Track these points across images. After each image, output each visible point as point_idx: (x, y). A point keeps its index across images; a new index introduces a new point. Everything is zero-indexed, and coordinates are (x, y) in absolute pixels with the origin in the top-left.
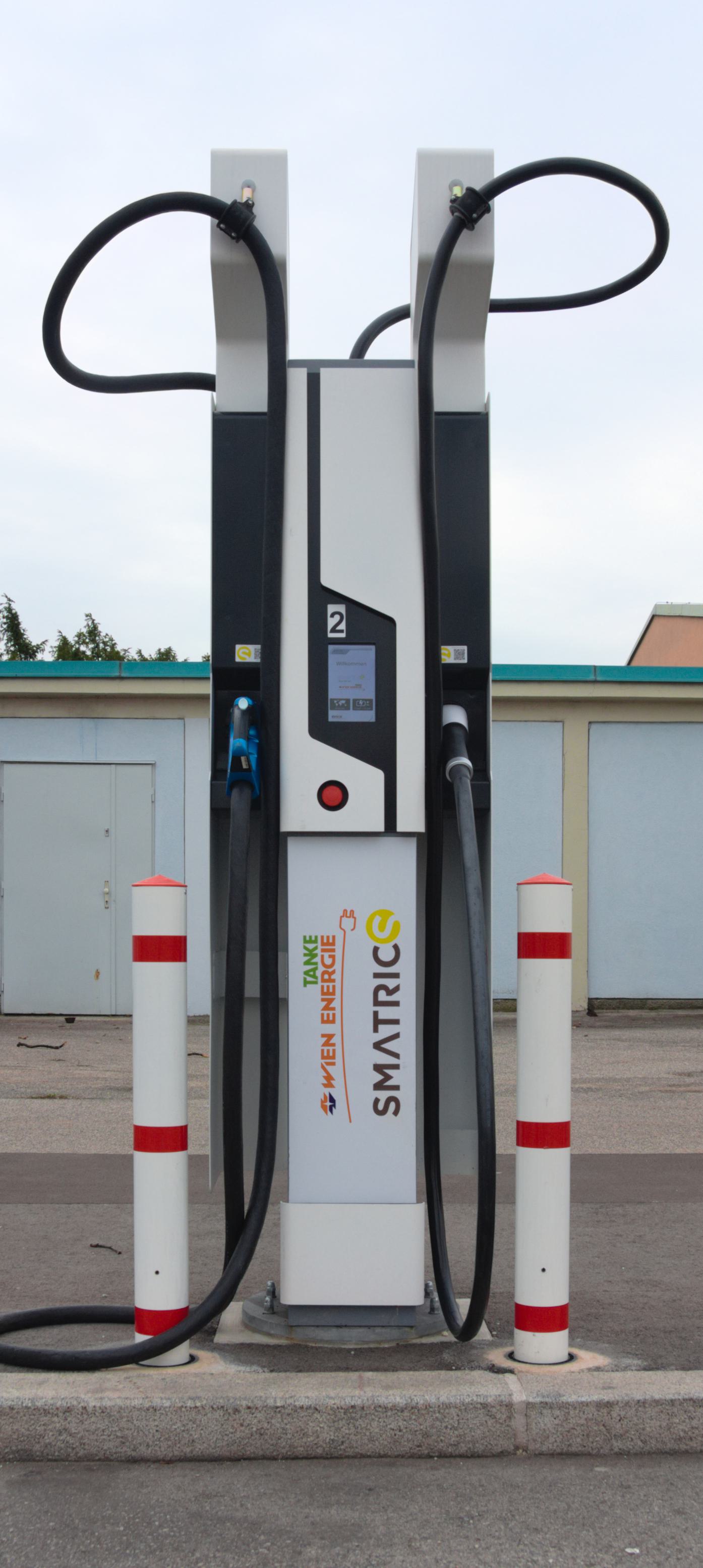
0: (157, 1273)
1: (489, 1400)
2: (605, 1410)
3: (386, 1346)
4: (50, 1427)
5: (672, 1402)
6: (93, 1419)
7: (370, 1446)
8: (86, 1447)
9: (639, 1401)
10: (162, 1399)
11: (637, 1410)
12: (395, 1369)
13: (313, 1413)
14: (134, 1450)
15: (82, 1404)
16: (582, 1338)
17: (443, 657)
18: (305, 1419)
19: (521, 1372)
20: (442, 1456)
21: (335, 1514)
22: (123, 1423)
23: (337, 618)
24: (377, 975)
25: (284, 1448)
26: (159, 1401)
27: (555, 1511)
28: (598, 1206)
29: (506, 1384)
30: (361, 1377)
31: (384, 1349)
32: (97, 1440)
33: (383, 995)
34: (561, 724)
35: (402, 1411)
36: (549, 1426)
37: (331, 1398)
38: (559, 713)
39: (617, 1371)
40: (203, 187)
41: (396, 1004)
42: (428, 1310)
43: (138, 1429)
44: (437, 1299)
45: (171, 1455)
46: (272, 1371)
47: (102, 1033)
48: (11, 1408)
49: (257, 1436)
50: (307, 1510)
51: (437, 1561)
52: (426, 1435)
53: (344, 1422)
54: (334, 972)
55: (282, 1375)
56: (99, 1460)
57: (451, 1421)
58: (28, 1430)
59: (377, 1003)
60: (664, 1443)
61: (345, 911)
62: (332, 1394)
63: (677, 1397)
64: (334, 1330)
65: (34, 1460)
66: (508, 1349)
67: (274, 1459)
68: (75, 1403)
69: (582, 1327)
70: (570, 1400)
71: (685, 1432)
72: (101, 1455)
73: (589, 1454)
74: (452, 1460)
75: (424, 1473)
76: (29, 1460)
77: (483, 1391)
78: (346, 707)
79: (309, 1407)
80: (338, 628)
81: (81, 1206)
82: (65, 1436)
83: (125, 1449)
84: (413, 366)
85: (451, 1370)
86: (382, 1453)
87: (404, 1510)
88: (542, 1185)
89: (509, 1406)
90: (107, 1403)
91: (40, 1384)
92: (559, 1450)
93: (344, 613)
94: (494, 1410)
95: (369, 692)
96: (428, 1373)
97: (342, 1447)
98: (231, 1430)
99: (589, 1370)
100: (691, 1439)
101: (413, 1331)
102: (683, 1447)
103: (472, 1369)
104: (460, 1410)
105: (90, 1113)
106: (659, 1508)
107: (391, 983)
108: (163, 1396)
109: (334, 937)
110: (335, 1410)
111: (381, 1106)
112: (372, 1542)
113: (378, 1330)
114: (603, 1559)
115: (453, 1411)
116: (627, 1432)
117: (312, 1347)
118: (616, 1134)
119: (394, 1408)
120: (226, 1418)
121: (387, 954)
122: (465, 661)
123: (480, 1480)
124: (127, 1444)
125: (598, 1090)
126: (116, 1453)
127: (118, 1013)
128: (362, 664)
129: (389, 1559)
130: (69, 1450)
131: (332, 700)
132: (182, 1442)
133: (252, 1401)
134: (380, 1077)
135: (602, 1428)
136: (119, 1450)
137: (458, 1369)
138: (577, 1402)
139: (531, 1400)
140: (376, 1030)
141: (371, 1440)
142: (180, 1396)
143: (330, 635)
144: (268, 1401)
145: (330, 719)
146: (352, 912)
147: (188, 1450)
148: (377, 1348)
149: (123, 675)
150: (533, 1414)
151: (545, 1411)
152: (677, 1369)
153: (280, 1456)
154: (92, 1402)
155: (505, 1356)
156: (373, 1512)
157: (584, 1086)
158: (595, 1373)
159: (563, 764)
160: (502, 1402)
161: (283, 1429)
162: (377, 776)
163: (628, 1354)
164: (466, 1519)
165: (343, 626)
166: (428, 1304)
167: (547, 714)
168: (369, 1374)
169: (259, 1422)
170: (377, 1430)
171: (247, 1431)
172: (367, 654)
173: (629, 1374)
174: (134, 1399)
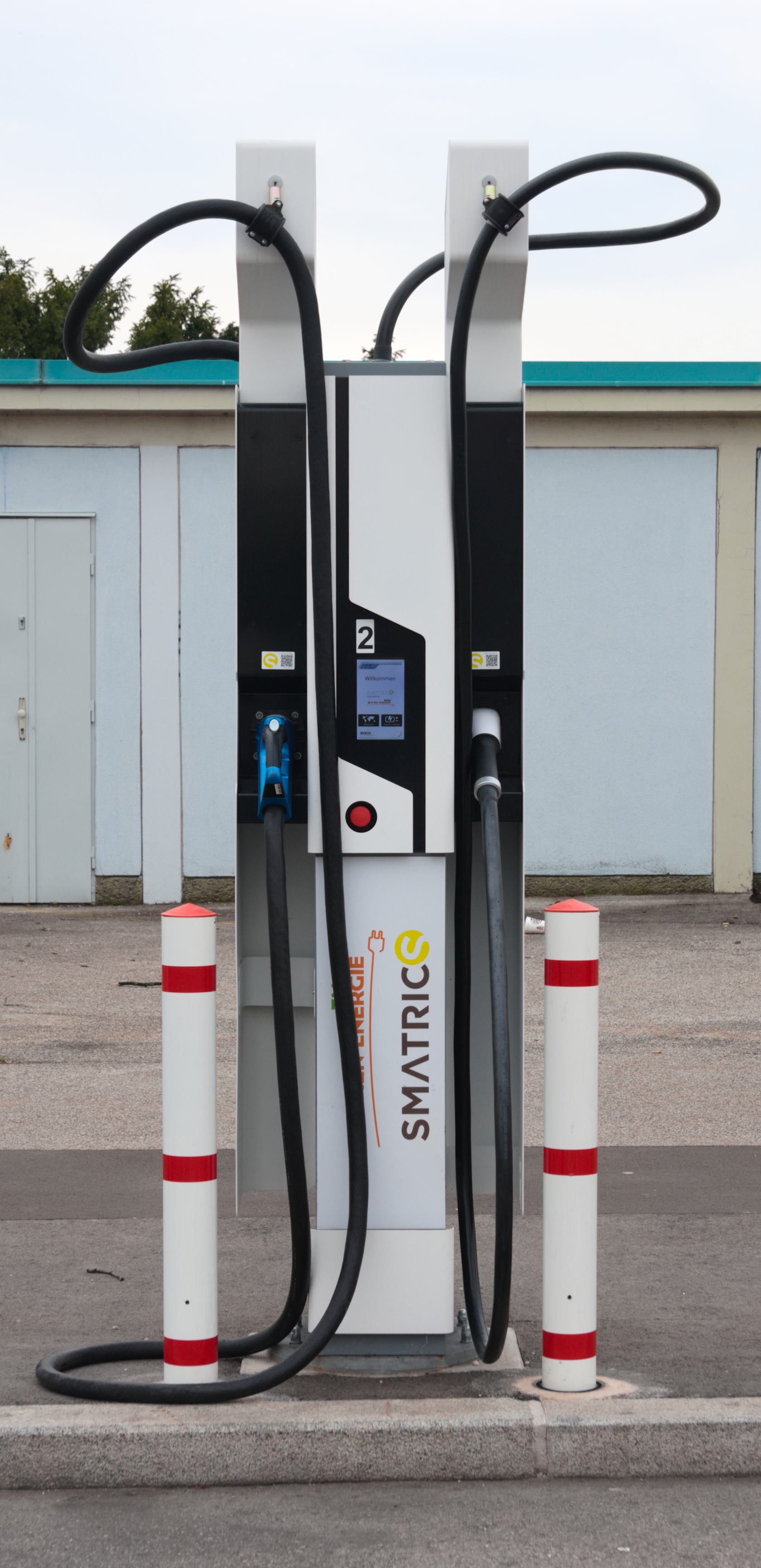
0: (187, 1302)
1: (511, 1424)
2: (622, 1434)
3: (415, 1375)
4: (90, 1455)
5: (687, 1426)
6: (131, 1447)
7: (397, 1469)
8: (124, 1474)
9: (654, 1426)
10: (197, 1425)
11: (652, 1434)
12: (422, 1397)
13: (342, 1438)
14: (171, 1476)
15: (121, 1432)
16: (617, 1367)
17: (473, 662)
18: (334, 1443)
19: (547, 1399)
20: (466, 1479)
21: (363, 1525)
22: (160, 1450)
23: (366, 633)
24: (405, 997)
25: (314, 1472)
26: (194, 1428)
27: (563, 1522)
28: (676, 1218)
29: (529, 1409)
30: (388, 1404)
31: (413, 1379)
32: (134, 1467)
33: (412, 1017)
34: (714, 452)
35: (427, 1435)
36: (568, 1449)
37: (359, 1423)
38: (712, 435)
39: (641, 1398)
40: (228, 193)
41: (425, 1026)
42: (460, 1339)
43: (175, 1456)
44: (468, 1327)
45: (205, 1480)
46: (301, 1400)
47: (25, 940)
48: (53, 1437)
49: (289, 1461)
50: (337, 1522)
51: (451, 1556)
52: (450, 1458)
53: (372, 1446)
54: (362, 994)
55: (312, 1403)
56: (137, 1486)
57: (474, 1445)
58: (69, 1458)
59: (405, 1025)
60: (679, 1466)
61: (374, 932)
62: (360, 1419)
63: (691, 1421)
64: (363, 1359)
65: (74, 1488)
66: (537, 1378)
67: (305, 1483)
68: (114, 1431)
69: (620, 1357)
70: (588, 1424)
71: (699, 1455)
72: (139, 1482)
73: (607, 1477)
74: (475, 1483)
75: (447, 1493)
76: (69, 1488)
77: (505, 1416)
78: (375, 723)
79: (338, 1432)
80: (367, 644)
81: (64, 1221)
82: (104, 1463)
83: (161, 1475)
84: (444, 373)
85: (478, 1397)
86: (408, 1476)
87: (425, 1521)
88: (569, 1211)
89: (530, 1430)
90: (146, 1431)
91: (76, 1414)
92: (577, 1473)
93: (373, 628)
94: (515, 1434)
95: (398, 708)
96: (455, 1400)
97: (370, 1471)
98: (264, 1455)
99: (614, 1397)
100: (705, 1462)
101: (443, 1360)
102: (698, 1470)
103: (498, 1396)
104: (483, 1434)
105: (43, 1088)
106: (659, 1519)
107: (420, 1005)
108: (198, 1423)
109: (362, 959)
110: (363, 1435)
111: (410, 1130)
112: (395, 1544)
113: (407, 1359)
114: (596, 1555)
115: (476, 1435)
116: (643, 1455)
117: (340, 1377)
118: (730, 1115)
119: (419, 1432)
120: (259, 1443)
121: (415, 976)
122: (498, 667)
123: (498, 1499)
124: (164, 1470)
125: (727, 1042)
126: (153, 1479)
127: (40, 901)
128: (390, 679)
129: (409, 1555)
130: (108, 1477)
131: (361, 716)
132: (217, 1467)
133: (284, 1427)
134: (409, 1101)
135: (619, 1451)
136: (156, 1476)
137: (484, 1396)
138: (595, 1426)
139: (551, 1424)
140: (404, 1052)
141: (398, 1463)
142: (214, 1422)
143: (359, 651)
144: (299, 1427)
145: (359, 737)
146: (381, 933)
147: (222, 1475)
148: (406, 1378)
149: (46, 381)
150: (552, 1438)
151: (564, 1435)
152: (701, 1397)
153: (311, 1480)
154: (130, 1429)
155: (533, 1385)
156: (397, 1523)
157: (710, 1036)
158: (619, 1400)
159: (717, 514)
160: (522, 1426)
161: (314, 1453)
162: (406, 796)
163: (656, 1382)
164: (481, 1527)
165: (371, 642)
166: (460, 1332)
167: (693, 436)
168: (397, 1402)
169: (290, 1447)
170: (403, 1454)
171: (279, 1456)
172: (396, 668)
173: (652, 1401)
174: (170, 1426)
